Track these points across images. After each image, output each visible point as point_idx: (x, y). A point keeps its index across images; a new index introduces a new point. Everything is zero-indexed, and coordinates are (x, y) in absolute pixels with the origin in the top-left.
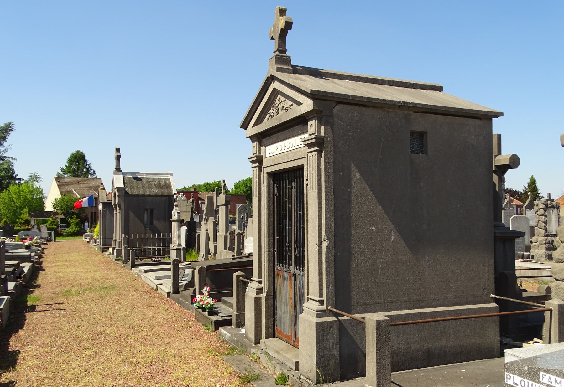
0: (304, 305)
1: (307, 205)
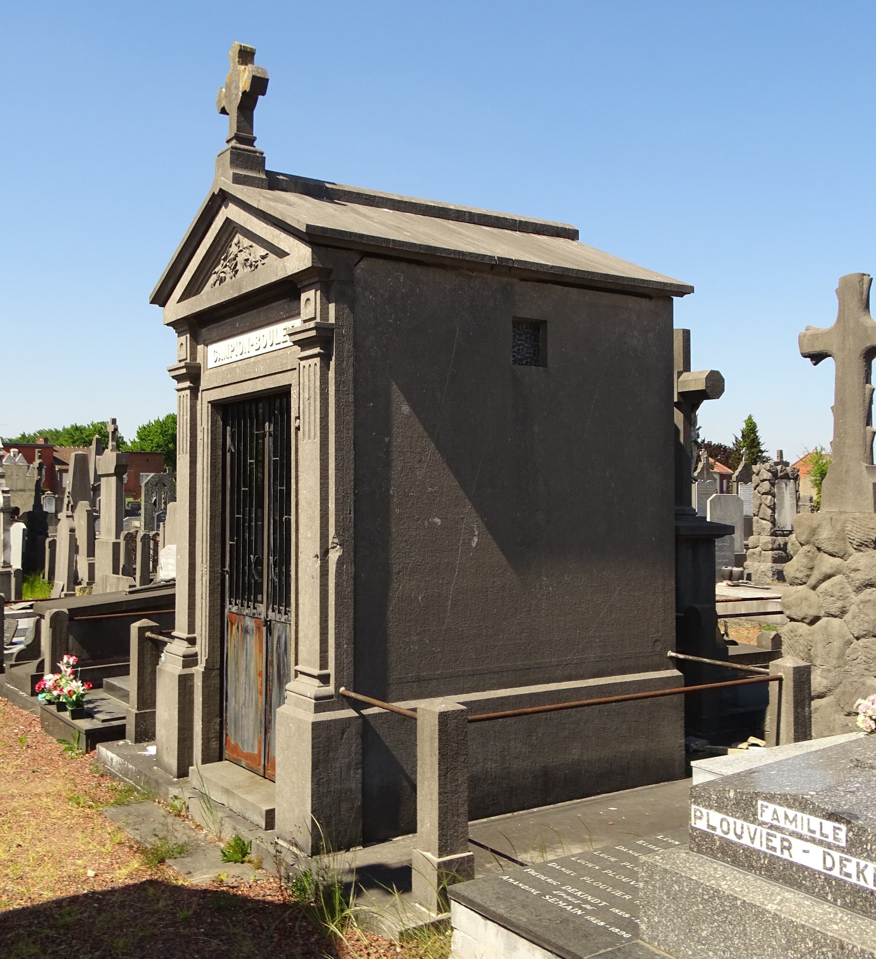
0: (288, 686)
1: (297, 471)
